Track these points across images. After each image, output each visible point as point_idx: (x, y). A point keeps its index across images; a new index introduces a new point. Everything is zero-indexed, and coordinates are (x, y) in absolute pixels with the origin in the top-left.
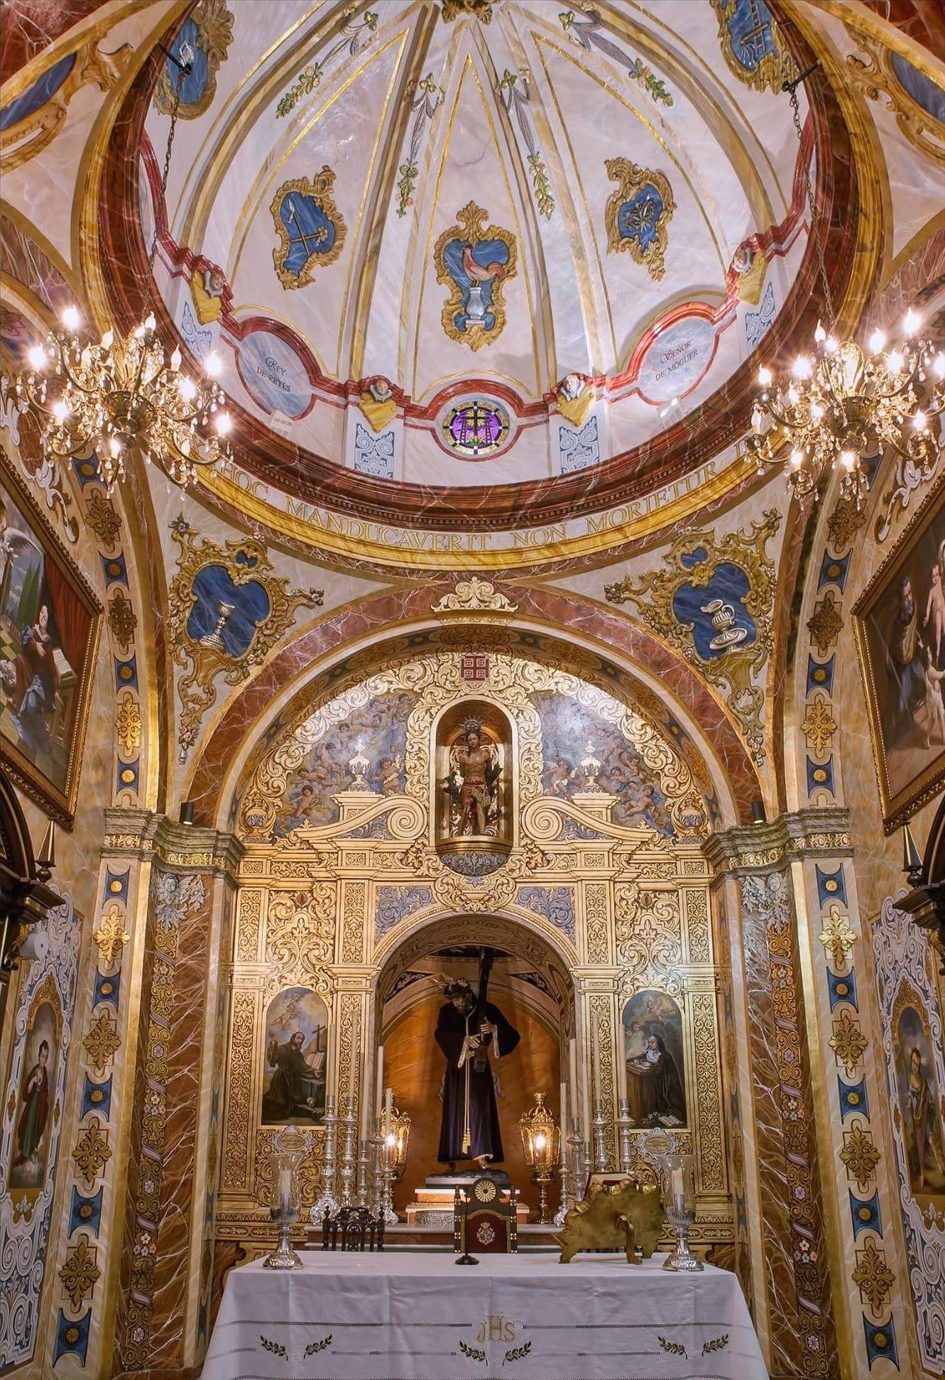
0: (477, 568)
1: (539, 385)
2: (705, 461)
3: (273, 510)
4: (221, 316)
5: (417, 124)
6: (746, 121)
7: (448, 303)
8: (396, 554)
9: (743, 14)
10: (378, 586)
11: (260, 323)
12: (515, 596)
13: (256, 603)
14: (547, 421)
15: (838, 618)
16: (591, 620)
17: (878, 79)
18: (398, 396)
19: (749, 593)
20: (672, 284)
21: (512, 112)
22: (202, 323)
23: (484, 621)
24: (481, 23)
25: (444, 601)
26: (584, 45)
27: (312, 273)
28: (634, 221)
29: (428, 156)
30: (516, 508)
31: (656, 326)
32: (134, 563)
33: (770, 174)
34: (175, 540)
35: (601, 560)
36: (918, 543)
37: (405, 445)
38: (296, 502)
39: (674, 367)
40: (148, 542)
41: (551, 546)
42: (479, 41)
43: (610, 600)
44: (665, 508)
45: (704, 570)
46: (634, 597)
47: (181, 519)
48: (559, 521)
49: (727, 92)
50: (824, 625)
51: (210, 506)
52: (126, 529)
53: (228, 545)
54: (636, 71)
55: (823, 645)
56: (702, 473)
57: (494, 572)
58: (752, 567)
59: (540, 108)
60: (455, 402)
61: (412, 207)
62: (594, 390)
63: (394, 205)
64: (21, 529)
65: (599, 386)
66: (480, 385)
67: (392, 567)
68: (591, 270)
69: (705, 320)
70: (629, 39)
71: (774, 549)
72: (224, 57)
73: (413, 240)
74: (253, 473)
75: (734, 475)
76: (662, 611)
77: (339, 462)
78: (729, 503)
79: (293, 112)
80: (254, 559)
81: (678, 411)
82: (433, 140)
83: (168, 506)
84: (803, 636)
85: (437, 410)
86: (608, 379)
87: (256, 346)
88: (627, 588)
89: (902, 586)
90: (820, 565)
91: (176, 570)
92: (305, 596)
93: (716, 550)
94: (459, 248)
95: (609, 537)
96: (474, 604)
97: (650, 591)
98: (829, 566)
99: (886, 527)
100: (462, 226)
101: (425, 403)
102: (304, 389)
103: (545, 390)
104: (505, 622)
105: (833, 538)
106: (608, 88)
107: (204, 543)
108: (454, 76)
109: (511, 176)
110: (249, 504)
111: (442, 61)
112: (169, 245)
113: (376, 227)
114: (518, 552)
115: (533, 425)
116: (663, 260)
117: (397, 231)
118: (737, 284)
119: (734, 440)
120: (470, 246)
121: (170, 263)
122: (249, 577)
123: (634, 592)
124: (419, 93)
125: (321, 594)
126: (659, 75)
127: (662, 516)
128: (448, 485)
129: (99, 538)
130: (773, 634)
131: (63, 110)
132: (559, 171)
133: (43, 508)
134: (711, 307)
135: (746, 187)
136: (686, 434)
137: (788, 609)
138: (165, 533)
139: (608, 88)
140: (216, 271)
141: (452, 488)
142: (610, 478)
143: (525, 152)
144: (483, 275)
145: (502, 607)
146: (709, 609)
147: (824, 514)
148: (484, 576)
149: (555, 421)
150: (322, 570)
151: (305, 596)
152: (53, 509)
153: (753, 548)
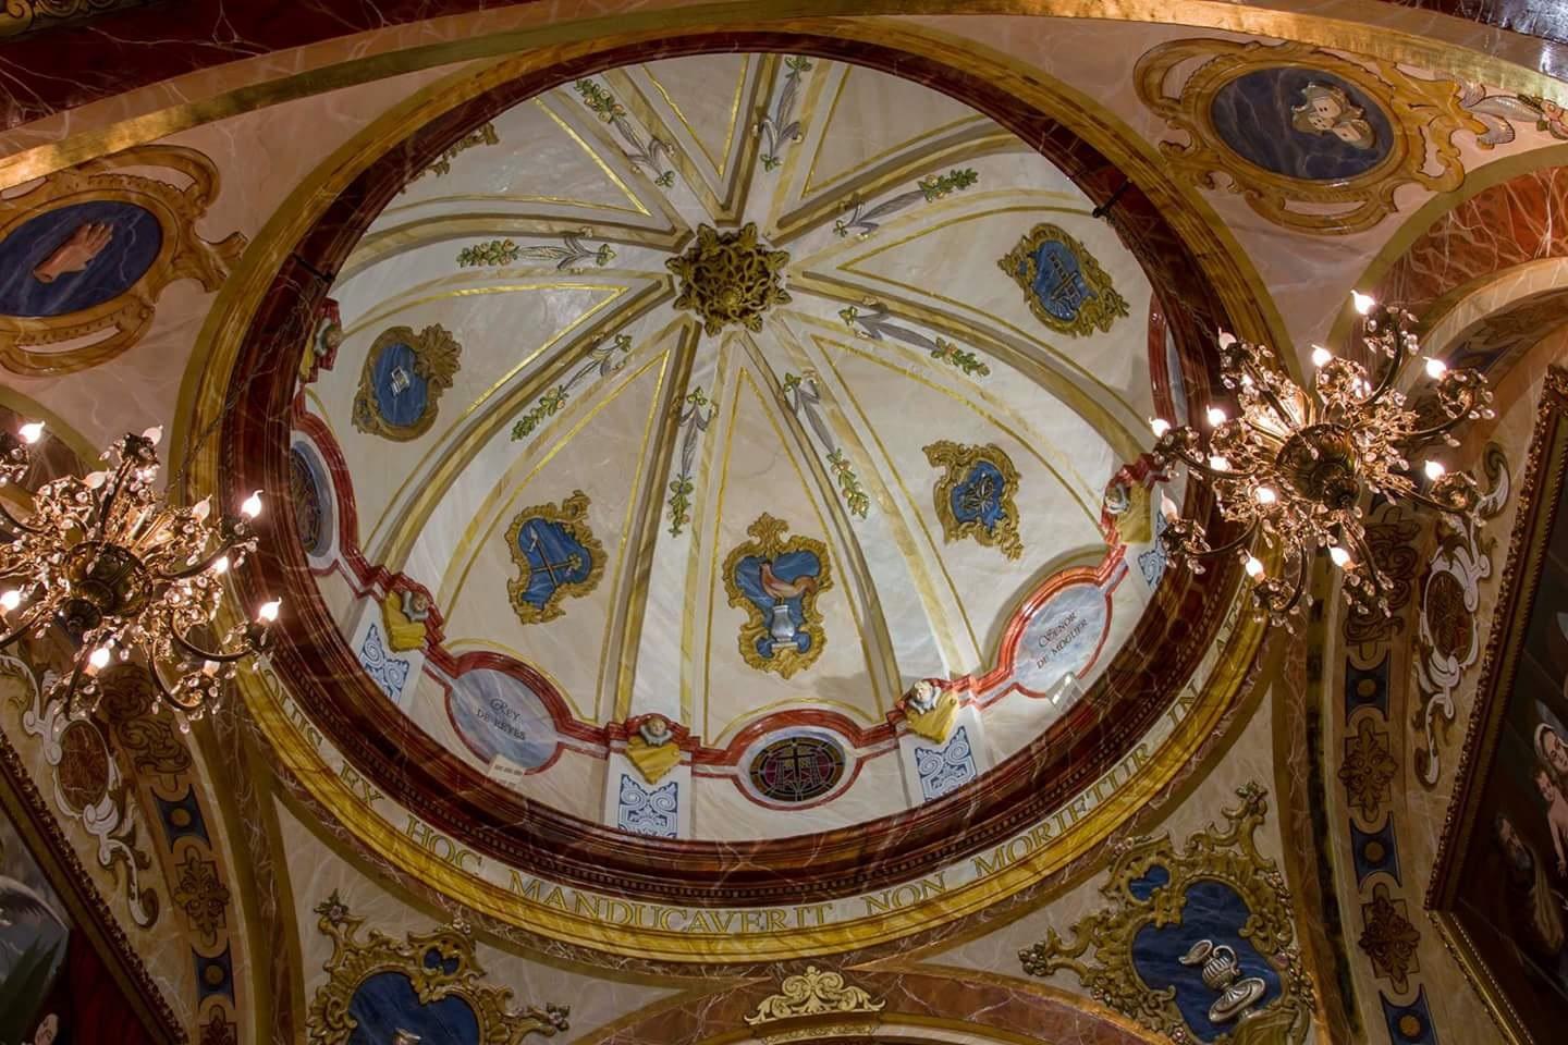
0: (814, 953)
1: (880, 706)
2: (1132, 744)
3: (487, 887)
4: (426, 645)
5: (687, 438)
6: (1081, 370)
7: (745, 627)
8: (684, 944)
9: (1046, 273)
10: (656, 993)
11: (483, 659)
12: (877, 986)
13: (457, 1031)
14: (897, 747)
15: (1404, 925)
16: (1007, 1008)
17: (1206, 156)
18: (681, 737)
19: (1250, 920)
20: (1034, 559)
21: (801, 414)
22: (394, 650)
23: (833, 1032)
24: (751, 333)
25: (764, 1007)
26: (874, 336)
27: (562, 605)
28: (971, 503)
29: (705, 472)
30: (865, 859)
31: (1025, 608)
32: (248, 962)
33: (1126, 411)
34: (323, 931)
35: (1004, 913)
36: (1495, 753)
37: (694, 800)
38: (526, 878)
39: (1059, 647)
40: (276, 933)
41: (923, 906)
42: (752, 351)
43: (1030, 972)
44: (1087, 820)
45: (1168, 899)
46: (1069, 961)
47: (334, 899)
48: (933, 870)
49: (1050, 348)
50: (1388, 939)
51: (382, 880)
52: (238, 906)
53: (411, 939)
54: (939, 350)
55: (1397, 973)
56: (1131, 763)
57: (840, 955)
58: (1242, 877)
59: (833, 406)
60: (761, 743)
61: (690, 525)
62: (955, 695)
63: (666, 524)
64: (28, 881)
65: (961, 690)
66: (797, 716)
67: (679, 964)
68: (928, 566)
69: (1086, 585)
70: (924, 323)
71: (1269, 843)
72: (449, 384)
73: (693, 562)
74: (459, 838)
75: (1177, 750)
76: (1118, 976)
77: (597, 821)
78: (1181, 790)
79: (533, 435)
80: (455, 961)
81: (1076, 691)
82: (709, 453)
83: (315, 878)
84: (1360, 966)
85: (740, 753)
86: (972, 680)
87: (479, 687)
88: (1055, 950)
89: (1495, 830)
90: (1348, 846)
91: (325, 978)
92: (538, 1017)
93: (1180, 863)
94: (753, 566)
95: (1011, 878)
96: (813, 1006)
97: (1092, 949)
98: (1364, 847)
99: (1434, 761)
100: (756, 540)
101: (723, 746)
102: (546, 736)
103: (889, 706)
104: (867, 1030)
105: (1355, 801)
106: (912, 375)
107: (372, 936)
108: (727, 392)
109: (811, 480)
110: (446, 878)
111: (711, 373)
112: (358, 563)
113: (644, 551)
114: (874, 921)
115: (877, 755)
116: (1017, 535)
117: (672, 552)
118: (1118, 529)
119: (1165, 707)
120: (769, 562)
121: (357, 583)
122: (444, 989)
123: (1068, 954)
124: (687, 407)
125: (565, 1013)
126: (966, 349)
127: (1085, 833)
128: (758, 838)
129: (193, 925)
130: (1310, 976)
131: (150, 310)
132: (868, 466)
133: (89, 865)
134: (1091, 568)
135: (1099, 430)
136: (1094, 714)
137: (1320, 929)
138: (307, 921)
139: (912, 375)
140: (419, 591)
141: (764, 842)
142: (996, 795)
143: (823, 452)
144: (788, 590)
145: (860, 1005)
146: (1193, 957)
147: (1330, 766)
148: (826, 963)
149: (907, 744)
150: (566, 974)
151: (538, 1017)
152: (110, 868)
153: (1236, 848)
